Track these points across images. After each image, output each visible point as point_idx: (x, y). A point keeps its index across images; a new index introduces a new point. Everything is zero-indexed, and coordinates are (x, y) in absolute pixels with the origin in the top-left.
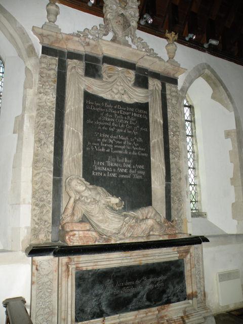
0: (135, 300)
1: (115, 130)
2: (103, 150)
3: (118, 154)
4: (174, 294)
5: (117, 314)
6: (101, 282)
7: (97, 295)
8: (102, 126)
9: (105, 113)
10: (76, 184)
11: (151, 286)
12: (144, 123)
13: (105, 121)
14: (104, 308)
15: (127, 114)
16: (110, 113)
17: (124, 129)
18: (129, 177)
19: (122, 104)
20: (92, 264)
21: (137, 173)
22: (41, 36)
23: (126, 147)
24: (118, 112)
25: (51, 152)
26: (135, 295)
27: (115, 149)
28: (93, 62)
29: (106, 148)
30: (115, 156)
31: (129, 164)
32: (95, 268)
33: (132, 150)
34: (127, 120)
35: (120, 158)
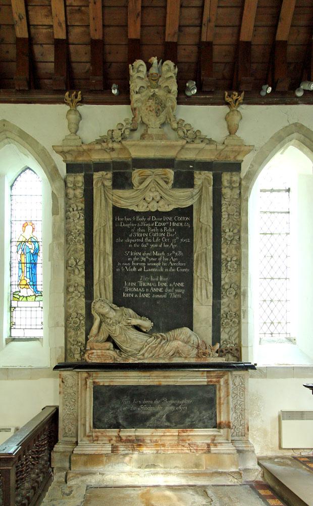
0: (152, 418)
1: (149, 246)
2: (134, 269)
3: (152, 272)
4: (201, 420)
5: (134, 428)
6: (118, 398)
7: (113, 409)
8: (133, 243)
9: (137, 228)
10: (103, 306)
11: (172, 408)
12: (187, 232)
13: (137, 238)
14: (120, 421)
15: (164, 224)
16: (142, 227)
17: (159, 243)
18: (165, 296)
19: (158, 214)
20: (108, 380)
21: (174, 291)
22: (62, 153)
23: (161, 264)
24: (153, 225)
25: (82, 277)
26: (153, 414)
27: (147, 267)
28: (121, 169)
29: (138, 267)
30: (148, 274)
31: (164, 282)
32: (112, 384)
33: (169, 267)
34: (163, 232)
35: (154, 277)
